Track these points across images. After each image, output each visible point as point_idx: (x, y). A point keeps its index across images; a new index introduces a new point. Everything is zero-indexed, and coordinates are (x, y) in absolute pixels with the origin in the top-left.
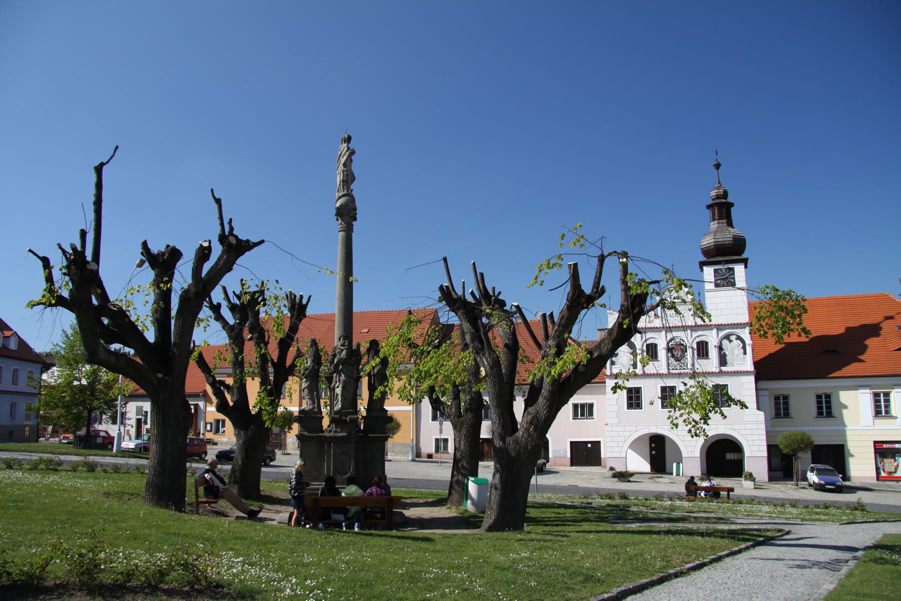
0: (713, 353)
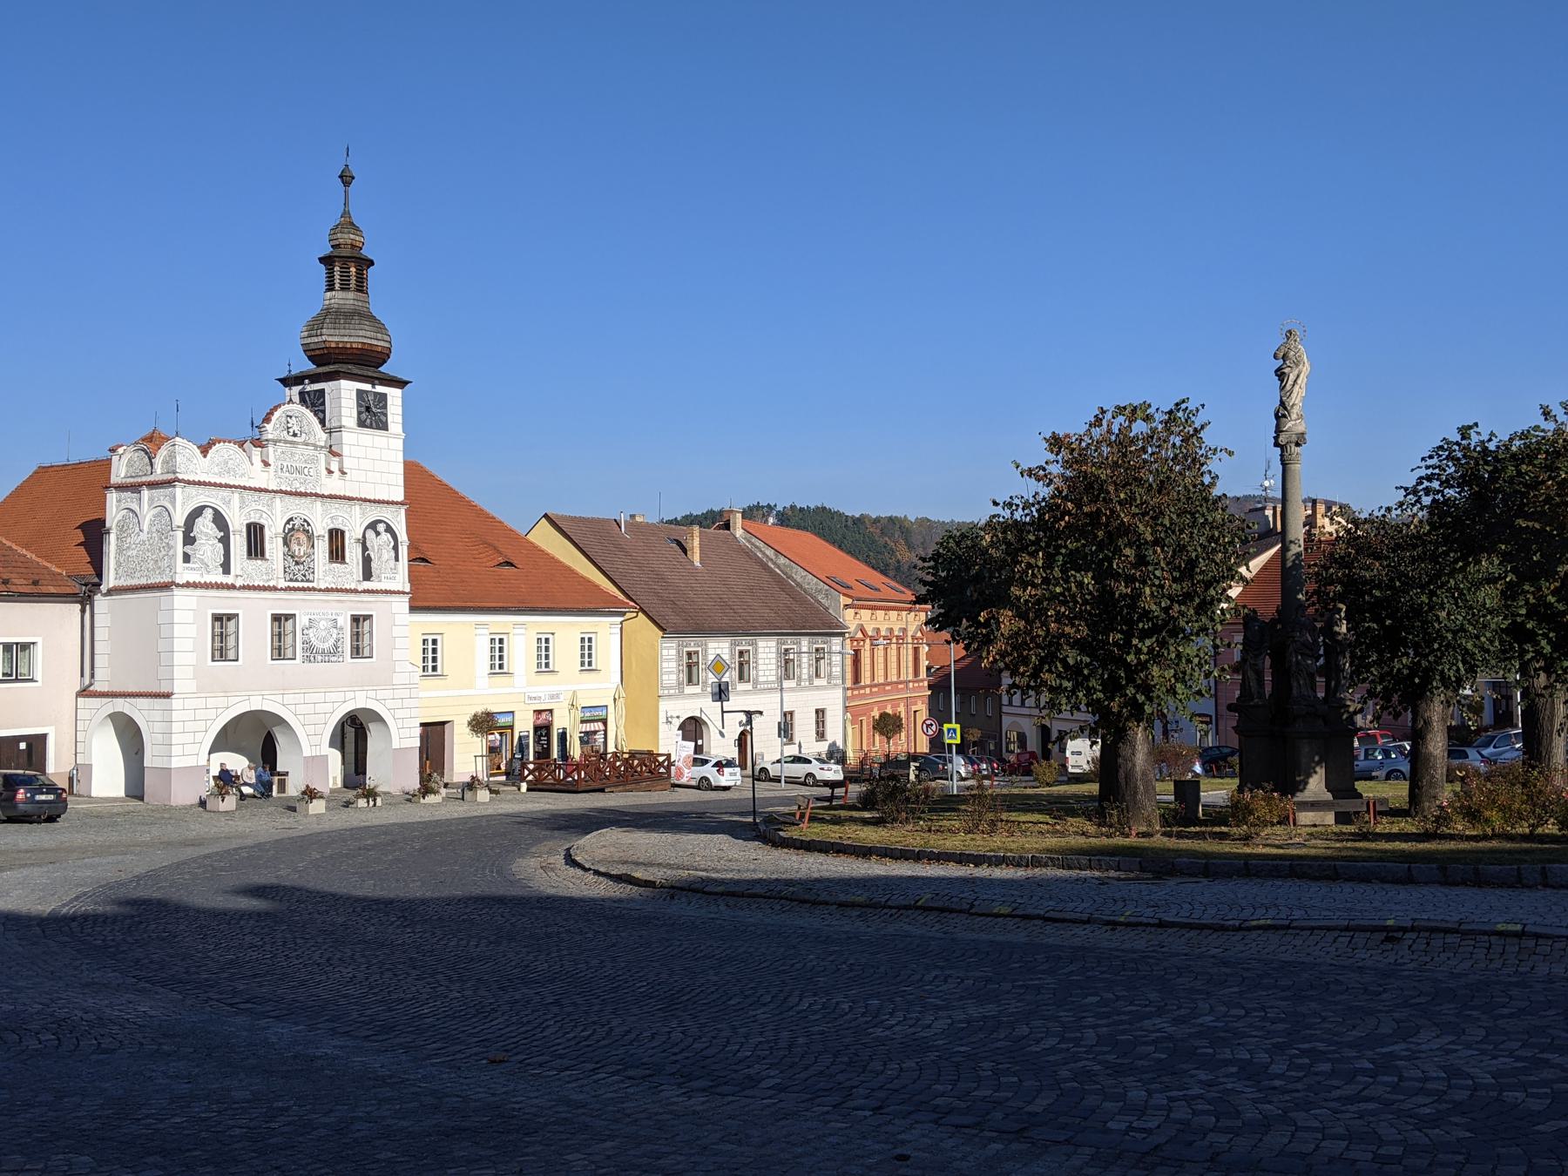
0: (353, 553)
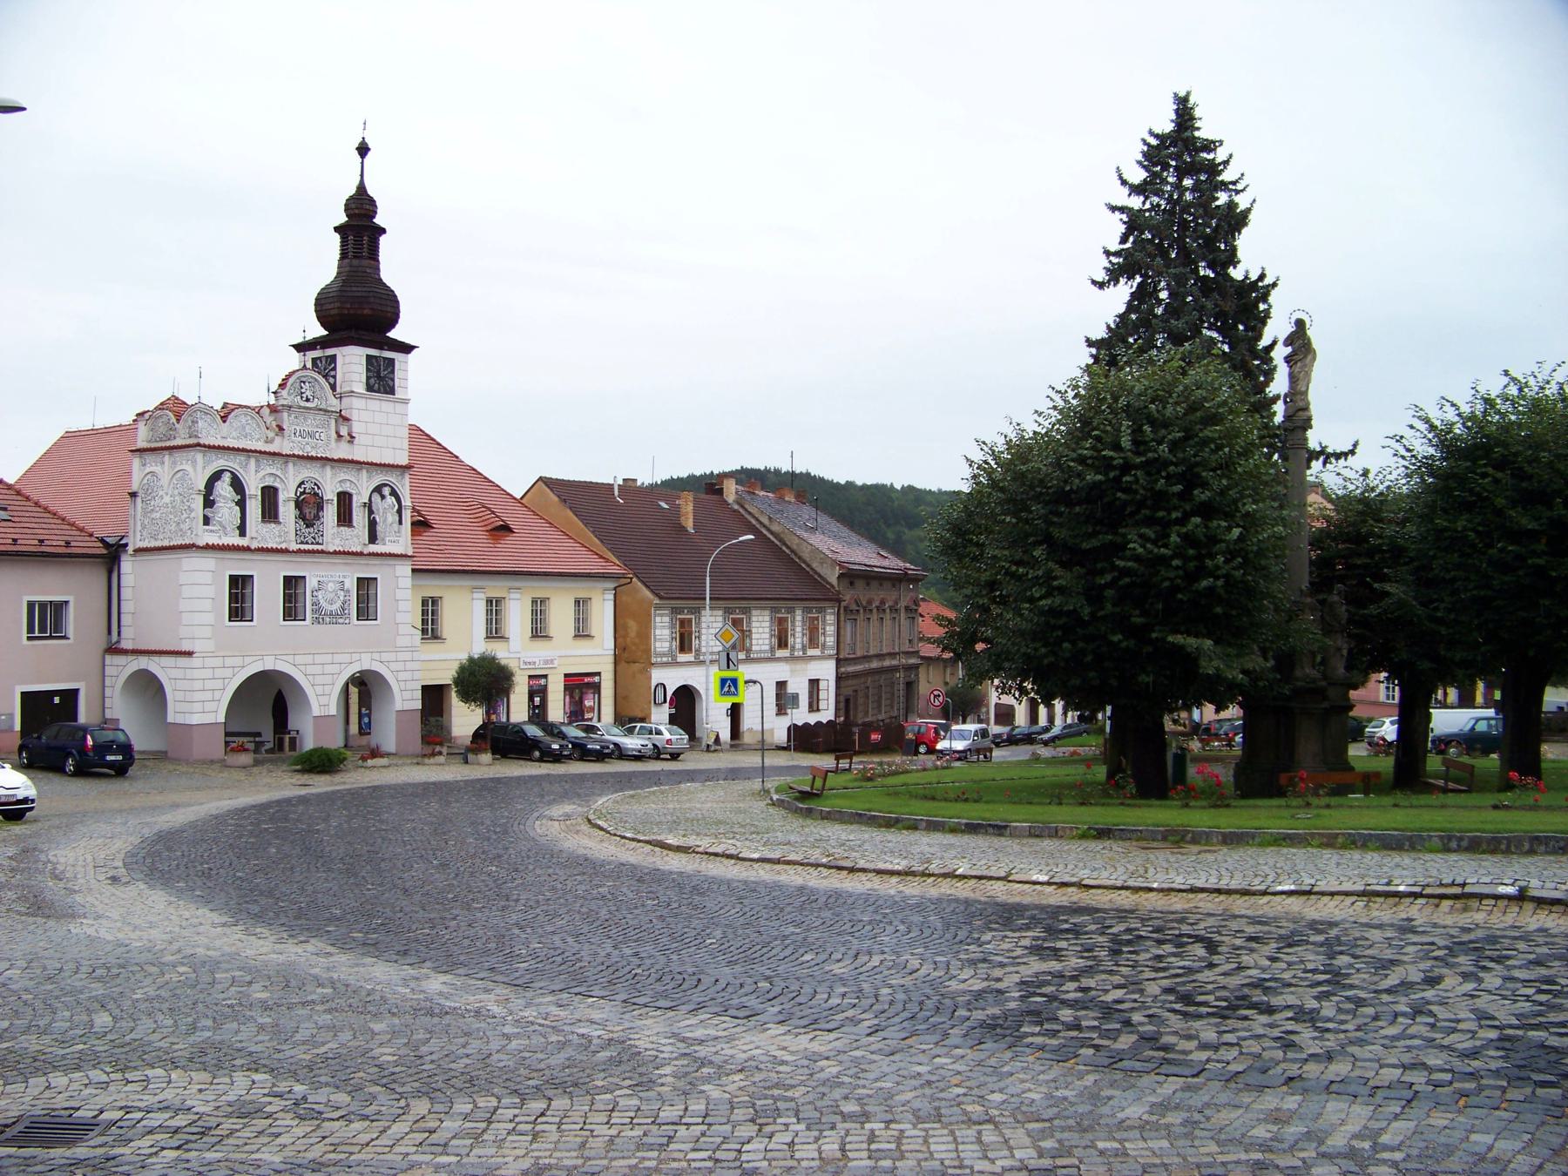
0: (359, 517)
